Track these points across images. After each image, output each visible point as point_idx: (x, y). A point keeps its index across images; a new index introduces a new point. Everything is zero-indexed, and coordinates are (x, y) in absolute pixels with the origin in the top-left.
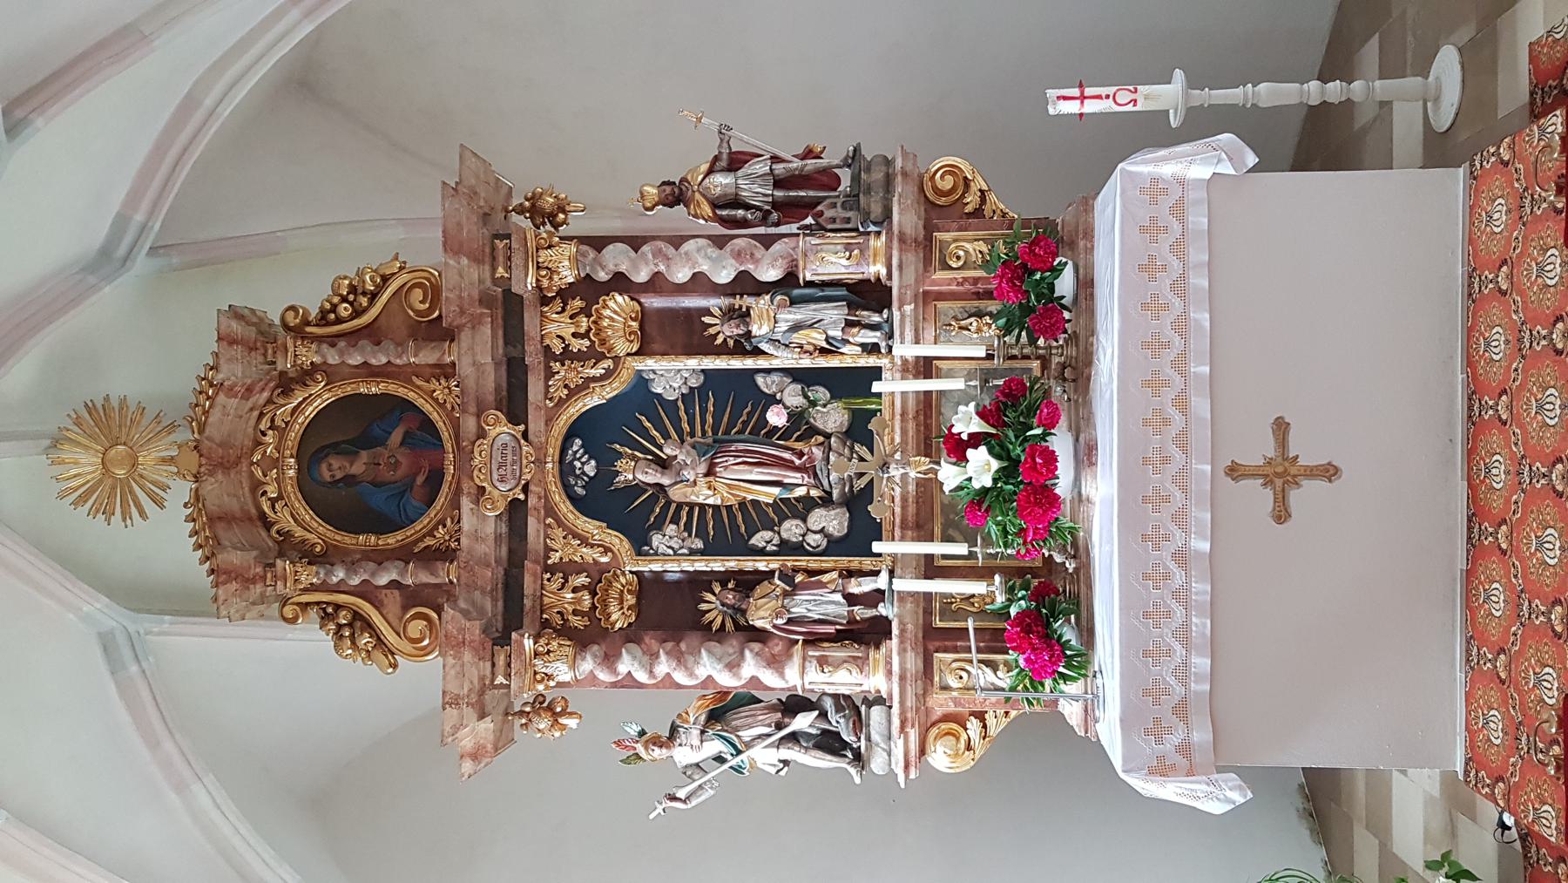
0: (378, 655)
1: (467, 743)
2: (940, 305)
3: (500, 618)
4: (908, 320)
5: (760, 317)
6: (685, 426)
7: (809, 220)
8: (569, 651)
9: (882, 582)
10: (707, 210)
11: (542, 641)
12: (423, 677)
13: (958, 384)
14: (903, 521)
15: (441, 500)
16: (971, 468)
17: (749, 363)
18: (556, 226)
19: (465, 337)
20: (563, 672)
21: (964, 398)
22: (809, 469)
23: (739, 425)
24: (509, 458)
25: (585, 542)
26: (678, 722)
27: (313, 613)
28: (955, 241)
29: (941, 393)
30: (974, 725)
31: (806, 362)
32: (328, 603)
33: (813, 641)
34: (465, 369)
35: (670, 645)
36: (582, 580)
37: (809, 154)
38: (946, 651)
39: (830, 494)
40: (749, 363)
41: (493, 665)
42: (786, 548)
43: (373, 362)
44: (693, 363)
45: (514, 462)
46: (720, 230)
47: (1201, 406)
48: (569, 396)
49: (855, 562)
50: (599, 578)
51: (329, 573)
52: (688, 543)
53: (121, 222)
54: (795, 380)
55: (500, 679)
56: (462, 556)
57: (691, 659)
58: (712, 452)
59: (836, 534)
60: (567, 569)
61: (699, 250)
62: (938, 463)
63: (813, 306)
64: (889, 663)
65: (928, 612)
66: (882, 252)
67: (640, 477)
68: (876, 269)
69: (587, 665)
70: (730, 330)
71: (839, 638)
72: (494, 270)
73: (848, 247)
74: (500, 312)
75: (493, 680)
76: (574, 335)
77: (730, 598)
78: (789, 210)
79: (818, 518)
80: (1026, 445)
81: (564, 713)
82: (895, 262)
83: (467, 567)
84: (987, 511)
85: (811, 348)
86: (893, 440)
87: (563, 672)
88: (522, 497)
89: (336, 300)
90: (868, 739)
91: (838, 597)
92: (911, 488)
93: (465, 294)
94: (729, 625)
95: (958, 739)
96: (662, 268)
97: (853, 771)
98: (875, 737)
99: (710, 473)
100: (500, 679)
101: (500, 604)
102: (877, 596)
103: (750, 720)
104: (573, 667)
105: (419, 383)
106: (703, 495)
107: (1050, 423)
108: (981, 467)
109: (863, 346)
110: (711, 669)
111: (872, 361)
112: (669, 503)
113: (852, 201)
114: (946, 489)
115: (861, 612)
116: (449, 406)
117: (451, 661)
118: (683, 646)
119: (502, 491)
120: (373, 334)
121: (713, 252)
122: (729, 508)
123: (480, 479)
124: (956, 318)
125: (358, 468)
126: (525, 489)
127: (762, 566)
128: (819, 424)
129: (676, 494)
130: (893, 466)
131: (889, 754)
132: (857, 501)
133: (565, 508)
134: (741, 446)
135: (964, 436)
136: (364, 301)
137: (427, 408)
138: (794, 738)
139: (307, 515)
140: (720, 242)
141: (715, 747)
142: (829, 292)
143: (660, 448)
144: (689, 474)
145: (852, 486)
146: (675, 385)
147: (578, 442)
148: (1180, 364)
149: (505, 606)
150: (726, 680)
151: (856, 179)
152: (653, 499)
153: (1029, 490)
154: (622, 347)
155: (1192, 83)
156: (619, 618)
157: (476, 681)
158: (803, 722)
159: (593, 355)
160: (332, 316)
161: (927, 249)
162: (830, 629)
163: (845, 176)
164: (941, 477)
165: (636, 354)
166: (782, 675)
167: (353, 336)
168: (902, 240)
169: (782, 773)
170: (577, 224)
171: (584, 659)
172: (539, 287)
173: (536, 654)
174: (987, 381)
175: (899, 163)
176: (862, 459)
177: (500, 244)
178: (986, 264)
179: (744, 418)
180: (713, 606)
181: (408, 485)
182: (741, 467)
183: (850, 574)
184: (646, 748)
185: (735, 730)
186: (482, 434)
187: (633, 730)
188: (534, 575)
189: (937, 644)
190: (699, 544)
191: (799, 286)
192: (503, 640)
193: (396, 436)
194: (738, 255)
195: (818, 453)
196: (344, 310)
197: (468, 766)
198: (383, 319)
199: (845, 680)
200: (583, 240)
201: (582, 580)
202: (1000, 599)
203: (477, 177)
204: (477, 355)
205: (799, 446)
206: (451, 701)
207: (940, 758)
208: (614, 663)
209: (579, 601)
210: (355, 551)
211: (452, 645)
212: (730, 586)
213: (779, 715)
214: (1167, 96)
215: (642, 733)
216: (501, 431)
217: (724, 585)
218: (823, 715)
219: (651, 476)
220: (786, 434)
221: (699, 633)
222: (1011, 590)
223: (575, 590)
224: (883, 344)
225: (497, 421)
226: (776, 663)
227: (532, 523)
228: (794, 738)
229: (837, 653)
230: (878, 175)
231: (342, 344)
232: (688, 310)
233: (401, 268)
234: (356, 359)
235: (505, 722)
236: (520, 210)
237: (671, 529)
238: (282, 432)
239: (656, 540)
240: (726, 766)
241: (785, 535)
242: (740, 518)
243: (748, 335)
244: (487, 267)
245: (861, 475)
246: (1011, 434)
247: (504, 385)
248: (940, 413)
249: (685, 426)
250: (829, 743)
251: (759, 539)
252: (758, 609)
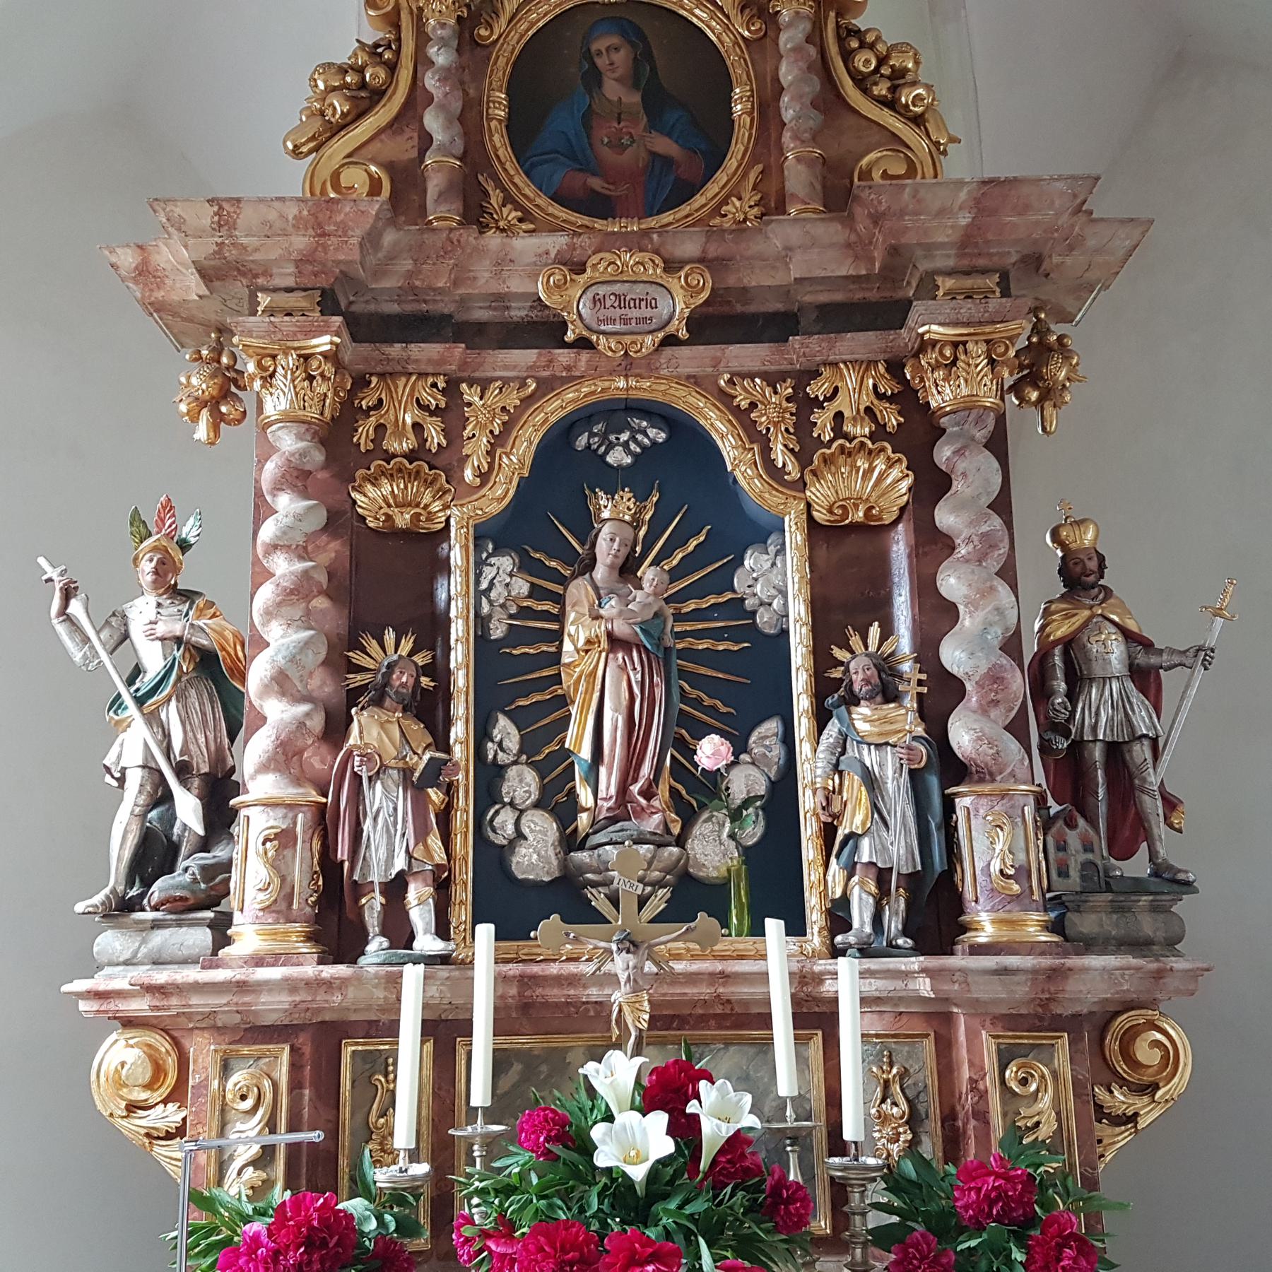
0: (317, 124)
2: (929, 1046)
3: (372, 307)
4: (899, 984)
5: (885, 720)
6: (691, 606)
7: (1055, 808)
8: (312, 413)
9: (427, 943)
10: (1061, 630)
11: (329, 369)
12: (271, 172)
13: (786, 1085)
14: (535, 980)
16: (628, 1119)
17: (802, 703)
18: (1016, 388)
19: (832, 231)
20: (276, 404)
22: (623, 809)
23: (693, 693)
24: (635, 313)
25: (498, 441)
26: (200, 602)
28: (1055, 1075)
29: (768, 1043)
31: (808, 801)
32: (398, 52)
33: (324, 822)
34: (781, 234)
35: (322, 578)
36: (435, 437)
37: (1171, 804)
38: (295, 1067)
39: (581, 847)
40: (802, 703)
41: (289, 290)
43: (786, 98)
44: (798, 610)
45: (626, 321)
46: (1030, 649)
48: (736, 411)
49: (463, 893)
50: (433, 465)
51: (443, 43)
52: (499, 614)
54: (773, 785)
55: (264, 300)
56: (469, 236)
57: (298, 612)
58: (649, 647)
59: (515, 860)
60: (451, 413)
61: (999, 611)
62: (637, 1052)
63: (910, 812)
64: (274, 959)
66: (1016, 935)
67: (606, 530)
68: (985, 925)
69: (288, 442)
70: (859, 671)
71: (329, 866)
72: (950, 273)
73: (1022, 873)
74: (873, 295)
75: (265, 290)
76: (839, 416)
77: (403, 678)
80: (679, 1239)
81: (218, 420)
82: (1013, 961)
83: (451, 246)
84: (548, 1154)
85: (836, 808)
86: (678, 957)
87: (276, 404)
88: (570, 336)
89: (881, 48)
90: (156, 925)
91: (400, 863)
92: (594, 993)
93: (908, 221)
94: (359, 679)
95: (149, 1086)
96: (963, 551)
97: (98, 899)
98: (159, 938)
99: (615, 642)
100: (264, 300)
101: (394, 308)
102: (400, 934)
103: (196, 720)
104: (287, 418)
105: (752, 176)
106: (578, 631)
108: (633, 1143)
109: (845, 901)
110: (277, 645)
111: (815, 917)
112: (564, 581)
113: (1099, 881)
114: (590, 1068)
115: (374, 905)
116: (717, 221)
117: (292, 211)
118: (321, 603)
119: (578, 306)
120: (830, 101)
121: (996, 635)
122: (557, 679)
123: (598, 266)
124: (904, 1074)
125: (612, 89)
126: (583, 344)
127: (458, 731)
128: (697, 830)
129: (579, 591)
130: (631, 959)
131: (123, 960)
132: (569, 896)
133: (555, 408)
134: (660, 692)
135: (692, 1107)
136: (881, 89)
137: (712, 189)
140: (1012, 646)
141: (153, 660)
142: (937, 839)
143: (656, 562)
144: (611, 607)
145: (595, 885)
146: (758, 589)
147: (661, 437)
149: (390, 317)
150: (259, 672)
151: (1137, 887)
152: (569, 556)
154: (819, 493)
156: (373, 499)
157: (256, 256)
158: (188, 809)
159: (805, 451)
160: (854, 44)
161: (1034, 1021)
162: (343, 852)
164: (615, 1058)
165: (810, 518)
166: (264, 768)
168: (1055, 974)
169: (108, 779)
170: (1025, 425)
171: (299, 437)
172: (925, 345)
173: (307, 358)
174: (795, 1141)
175: (1178, 964)
176: (642, 901)
177: (991, 281)
179: (707, 701)
180: (391, 652)
181: (583, 161)
182: (625, 694)
183: (442, 886)
184: (155, 549)
185: (181, 696)
186: (671, 266)
187: (189, 530)
188: (442, 361)
189: (307, 1050)
190: (498, 631)
191: (943, 787)
192: (328, 303)
193: (664, 145)
194: (994, 678)
195: (652, 823)
196: (865, 62)
197: (127, 259)
198: (851, 120)
199: (252, 879)
201: (435, 437)
202: (382, 1177)
203: (1097, 251)
204: (802, 253)
205: (663, 791)
206: (225, 212)
207: (120, 1054)
208: (293, 487)
209: (400, 433)
210: (480, 90)
211: (322, 204)
212: (425, 681)
213: (205, 769)
215: (184, 546)
216: (677, 303)
217: (426, 670)
218: (205, 845)
219: (606, 548)
221: (344, 631)
222: (396, 1197)
223: (417, 427)
224: (851, 938)
225: (692, 290)
226: (286, 757)
227: (525, 357)
228: (162, 798)
229: (301, 864)
230: (1148, 925)
231: (813, 51)
233: (937, 144)
234: (787, 73)
235: (206, 325)
237: (521, 586)
239: (506, 563)
240: (122, 688)
241: (512, 772)
242: (539, 698)
243: (852, 700)
244: (951, 263)
245: (614, 900)
246: (698, 1206)
247: (752, 308)
248: (728, 1043)
249: (691, 606)
250: (154, 854)
251: (504, 729)
252: (382, 725)
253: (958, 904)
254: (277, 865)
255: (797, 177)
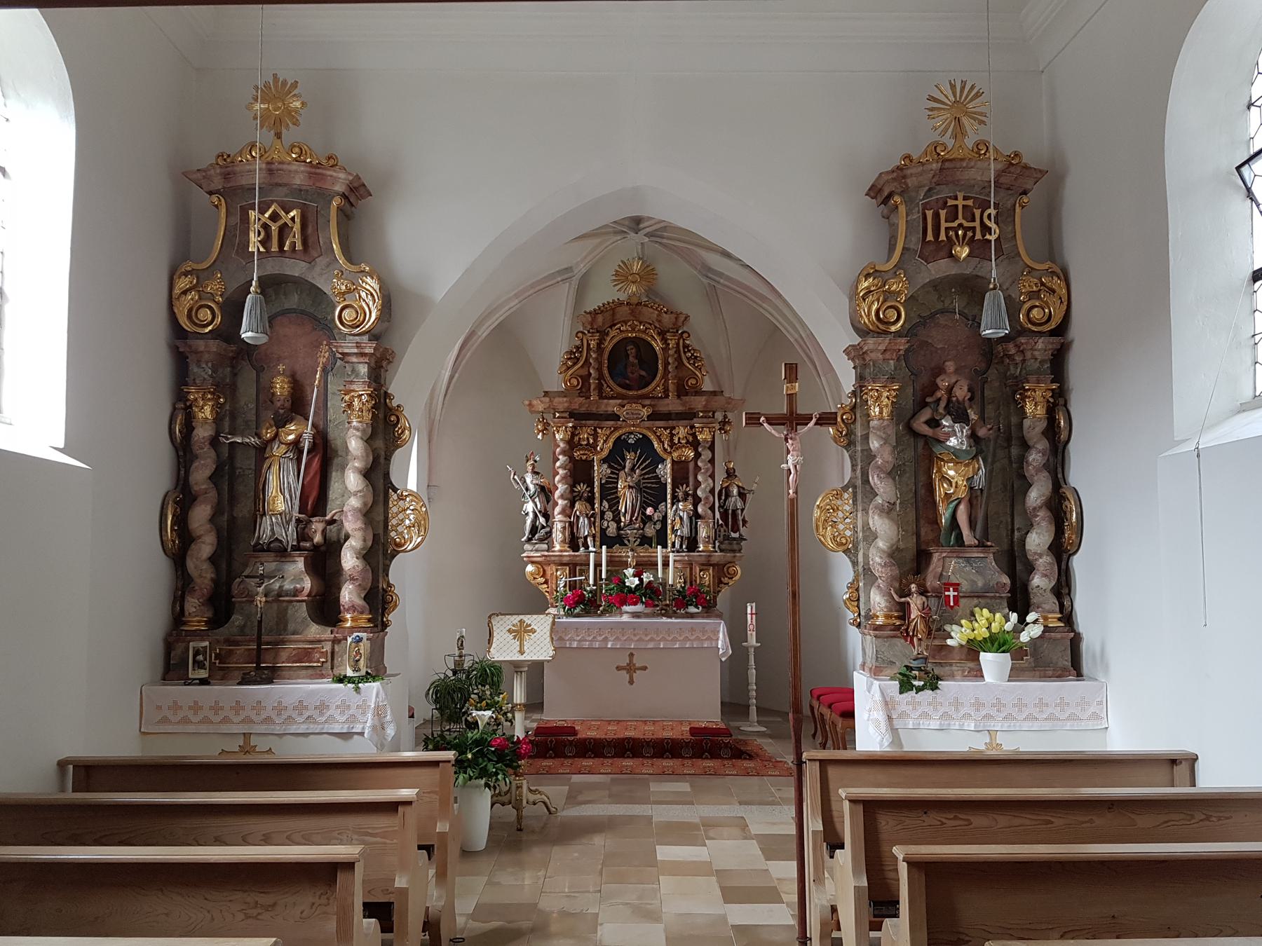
1: (535, 402)
9: (591, 549)
12: (555, 381)
13: (660, 575)
15: (620, 389)
21: (655, 576)
27: (578, 343)
30: (542, 580)
33: (571, 524)
34: (666, 401)
37: (744, 522)
42: (603, 513)
47: (651, 645)
49: (598, 539)
53: (721, 275)
58: (637, 487)
65: (581, 565)
70: (680, 495)
71: (572, 533)
78: (724, 515)
79: (613, 525)
99: (630, 487)
107: (647, 605)
108: (633, 582)
113: (727, 538)
119: (623, 413)
120: (680, 364)
125: (631, 359)
129: (622, 474)
131: (529, 551)
132: (619, 540)
133: (617, 434)
137: (653, 385)
138: (536, 516)
139: (615, 341)
140: (712, 491)
148: (664, 639)
150: (557, 494)
153: (625, 596)
154: (675, 455)
155: (756, 648)
158: (542, 520)
159: (672, 445)
161: (706, 565)
163: (733, 535)
167: (679, 359)
178: (701, 584)
180: (582, 488)
183: (594, 536)
193: (643, 373)
194: (707, 498)
199: (557, 535)
200: (713, 442)
204: (672, 404)
207: (530, 568)
214: (752, 640)
216: (645, 412)
218: (543, 527)
220: (644, 514)
226: (563, 512)
230: (735, 547)
232: (688, 478)
234: (670, 360)
236: (725, 417)
238: (644, 332)
239: (605, 466)
250: (534, 530)
253: (697, 542)
254: (563, 533)
255: (671, 387)
